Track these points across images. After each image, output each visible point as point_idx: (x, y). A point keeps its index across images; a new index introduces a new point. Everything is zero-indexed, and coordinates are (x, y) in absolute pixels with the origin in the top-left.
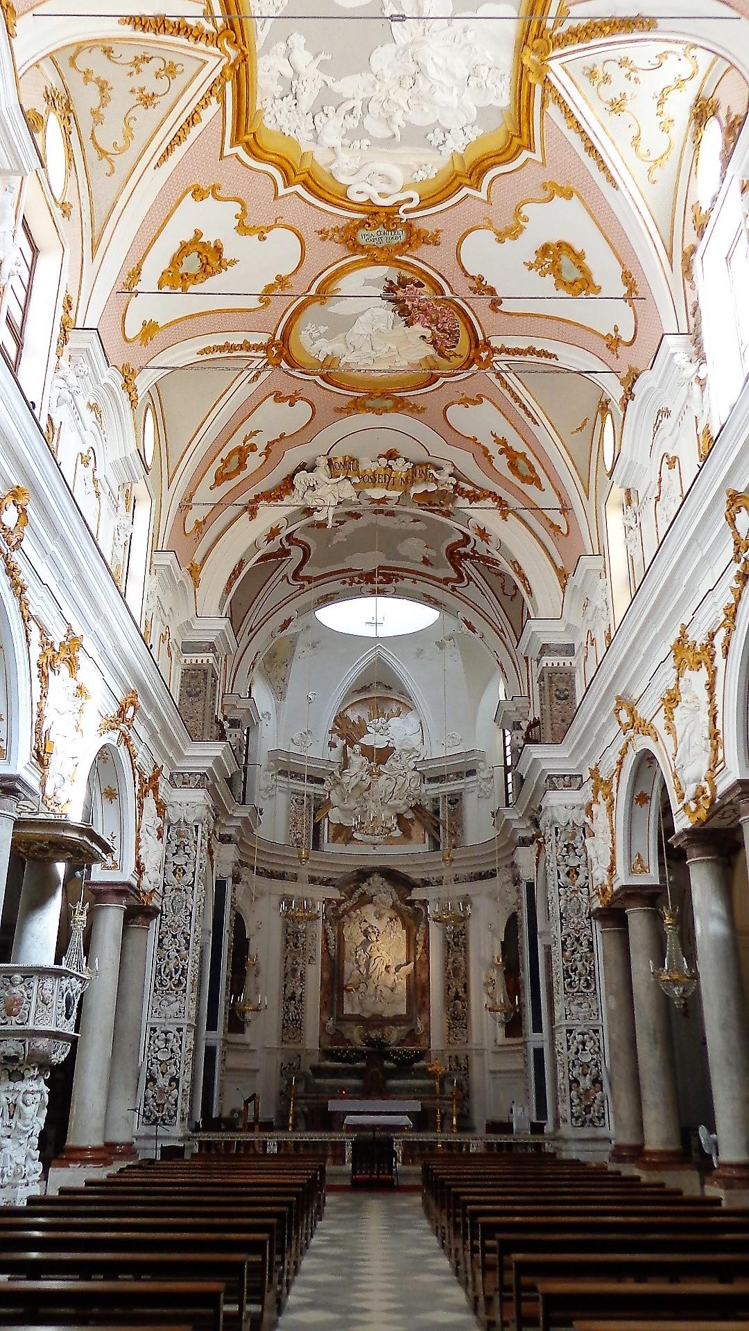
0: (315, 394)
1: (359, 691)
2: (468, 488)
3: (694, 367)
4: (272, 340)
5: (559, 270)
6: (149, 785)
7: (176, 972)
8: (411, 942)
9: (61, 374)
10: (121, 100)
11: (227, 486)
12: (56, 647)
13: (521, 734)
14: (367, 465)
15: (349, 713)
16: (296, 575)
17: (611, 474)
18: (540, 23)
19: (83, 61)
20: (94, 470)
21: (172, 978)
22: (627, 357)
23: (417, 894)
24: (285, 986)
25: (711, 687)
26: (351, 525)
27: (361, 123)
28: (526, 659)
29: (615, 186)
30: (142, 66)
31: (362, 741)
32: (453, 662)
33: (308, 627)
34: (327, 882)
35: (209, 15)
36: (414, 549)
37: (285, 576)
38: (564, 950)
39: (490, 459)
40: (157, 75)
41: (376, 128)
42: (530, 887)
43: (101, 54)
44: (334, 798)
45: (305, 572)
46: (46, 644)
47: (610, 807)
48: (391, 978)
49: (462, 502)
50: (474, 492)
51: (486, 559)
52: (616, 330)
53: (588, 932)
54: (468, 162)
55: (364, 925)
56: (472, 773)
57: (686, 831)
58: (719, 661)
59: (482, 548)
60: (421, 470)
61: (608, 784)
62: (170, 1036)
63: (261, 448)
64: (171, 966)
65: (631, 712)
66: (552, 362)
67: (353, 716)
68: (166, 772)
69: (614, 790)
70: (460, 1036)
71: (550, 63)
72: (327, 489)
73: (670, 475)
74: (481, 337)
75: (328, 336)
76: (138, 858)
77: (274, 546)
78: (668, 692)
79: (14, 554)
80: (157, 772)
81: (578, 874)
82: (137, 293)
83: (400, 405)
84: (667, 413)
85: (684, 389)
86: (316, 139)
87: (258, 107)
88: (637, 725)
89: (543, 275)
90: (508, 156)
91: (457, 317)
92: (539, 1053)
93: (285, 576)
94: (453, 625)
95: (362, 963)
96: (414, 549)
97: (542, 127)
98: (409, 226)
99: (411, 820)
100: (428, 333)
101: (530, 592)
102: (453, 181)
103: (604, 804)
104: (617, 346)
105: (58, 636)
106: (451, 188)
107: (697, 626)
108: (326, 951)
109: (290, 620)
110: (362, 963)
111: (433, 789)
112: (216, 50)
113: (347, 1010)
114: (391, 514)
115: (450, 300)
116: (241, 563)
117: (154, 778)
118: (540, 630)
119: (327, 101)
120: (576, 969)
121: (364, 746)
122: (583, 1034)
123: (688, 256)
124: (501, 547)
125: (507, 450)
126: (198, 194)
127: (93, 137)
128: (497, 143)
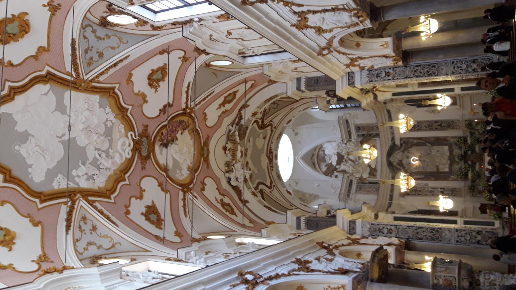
2: (237, 120)
4: (182, 190)
5: (158, 80)
7: (432, 232)
9: (195, 262)
10: (93, 237)
11: (236, 210)
14: (229, 158)
18: (72, 83)
19: (81, 250)
20: (231, 254)
21: (435, 234)
22: (191, 54)
23: (398, 142)
25: (315, 12)
26: (251, 165)
27: (103, 151)
29: (128, 56)
32: (303, 130)
33: (290, 185)
35: (66, 203)
36: (261, 143)
37: (270, 192)
39: (226, 111)
40: (85, 223)
41: (106, 146)
42: (394, 94)
43: (78, 243)
44: (358, 176)
45: (268, 184)
46: (299, 270)
47: (361, 58)
49: (243, 122)
50: (239, 118)
51: (264, 115)
53: (412, 67)
54: (119, 113)
56: (347, 121)
59: (259, 116)
60: (230, 137)
61: (352, 60)
63: (222, 197)
64: (430, 234)
65: (324, 49)
66: (191, 84)
67: (324, 169)
69: (354, 57)
71: (85, 79)
72: (237, 173)
73: (235, 34)
74: (182, 112)
75: (181, 169)
77: (259, 195)
78: (316, 32)
81: (388, 72)
82: (164, 237)
83: (206, 144)
84: (211, 36)
86: (109, 169)
87: (97, 188)
89: (159, 86)
90: (116, 97)
91: (174, 120)
92: (463, 89)
93: (270, 192)
94: (289, 129)
96: (261, 143)
97: (107, 83)
98: (141, 136)
100: (180, 132)
101: (276, 96)
102: (125, 118)
103: (360, 61)
104: (186, 58)
106: (127, 119)
109: (287, 191)
112: (78, 201)
113: (447, 170)
114: (246, 150)
115: (169, 121)
116: (265, 206)
118: (292, 91)
119: (95, 163)
120: (428, 71)
121: (337, 164)
122: (454, 68)
123: (155, 28)
124: (259, 107)
125: (223, 104)
126: (128, 212)
127: (107, 249)
128: (112, 101)
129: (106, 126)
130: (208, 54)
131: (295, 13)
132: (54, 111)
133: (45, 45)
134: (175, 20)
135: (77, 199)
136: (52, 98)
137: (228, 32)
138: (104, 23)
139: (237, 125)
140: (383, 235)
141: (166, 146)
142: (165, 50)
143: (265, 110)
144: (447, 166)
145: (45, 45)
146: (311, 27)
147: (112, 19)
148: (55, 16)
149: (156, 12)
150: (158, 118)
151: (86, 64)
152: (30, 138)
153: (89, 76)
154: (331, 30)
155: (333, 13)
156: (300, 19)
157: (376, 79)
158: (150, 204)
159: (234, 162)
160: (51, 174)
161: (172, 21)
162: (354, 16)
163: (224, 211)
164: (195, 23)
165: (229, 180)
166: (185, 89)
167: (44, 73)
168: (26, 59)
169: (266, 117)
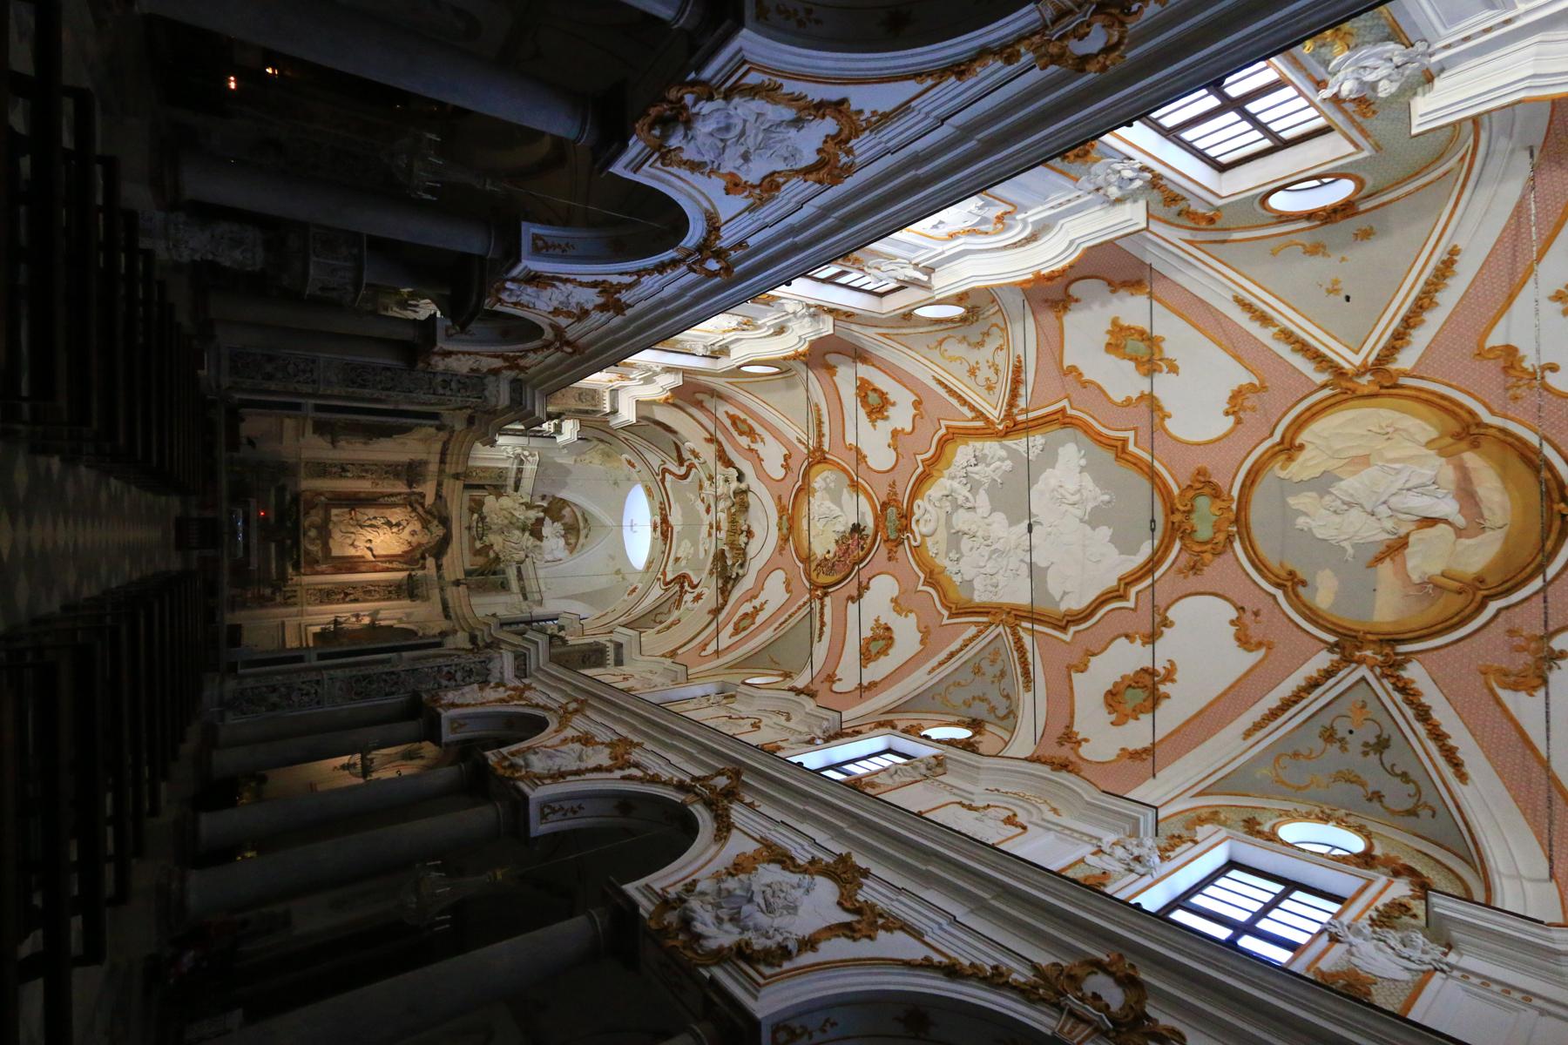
0: (789, 480)
1: (583, 515)
2: (729, 587)
3: (821, 735)
4: (823, 452)
6: (513, 364)
7: (363, 380)
8: (391, 558)
11: (728, 423)
12: (618, 295)
13: (556, 632)
15: (568, 509)
16: (665, 471)
17: (744, 683)
23: (430, 562)
24: (353, 464)
25: (598, 769)
26: (702, 508)
28: (611, 632)
30: (992, 369)
31: (547, 518)
34: (439, 496)
38: (387, 673)
42: (439, 645)
48: (361, 544)
52: (840, 680)
55: (404, 523)
57: (485, 759)
58: (618, 774)
59: (688, 597)
60: (742, 553)
61: (521, 698)
62: (308, 375)
63: (753, 446)
65: (576, 711)
66: (816, 639)
68: (522, 376)
69: (516, 702)
70: (313, 598)
73: (746, 725)
74: (830, 590)
76: (456, 353)
77: (686, 455)
78: (593, 737)
79: (685, 267)
80: (523, 369)
81: (449, 680)
83: (785, 539)
84: (788, 719)
85: (807, 730)
88: (565, 717)
89: (872, 629)
95: (374, 522)
96: (682, 548)
99: (487, 555)
100: (831, 555)
105: (625, 296)
107: (772, 828)
108: (384, 495)
110: (374, 522)
111: (512, 573)
112: (1002, 417)
113: (334, 511)
117: (517, 367)
121: (543, 519)
122: (316, 692)
125: (757, 611)
126: (917, 404)
127: (949, 337)
128: (952, 595)
129: (958, 550)
130: (791, 689)
131: (637, 765)
132: (1048, 568)
133: (1076, 677)
134: (854, 739)
135: (1002, 420)
136: (1054, 586)
137: (759, 727)
138: (976, 725)
139: (730, 577)
140: (458, 377)
141: (856, 528)
142: (865, 690)
143: (678, 607)
144: (334, 519)
145: (1076, 677)
146: (603, 743)
147: (963, 733)
148: (1064, 725)
149: (889, 751)
150: (871, 575)
151: (1001, 651)
152: (1087, 517)
153: (992, 632)
154: (564, 741)
155: (563, 769)
156: (626, 757)
157: (472, 666)
158: (880, 423)
159: (733, 510)
160: (1049, 457)
161: (860, 736)
162: (521, 767)
163: (750, 421)
164: (821, 735)
165: (741, 477)
166: (827, 629)
167: (1072, 629)
168: (1105, 649)
169: (676, 597)
